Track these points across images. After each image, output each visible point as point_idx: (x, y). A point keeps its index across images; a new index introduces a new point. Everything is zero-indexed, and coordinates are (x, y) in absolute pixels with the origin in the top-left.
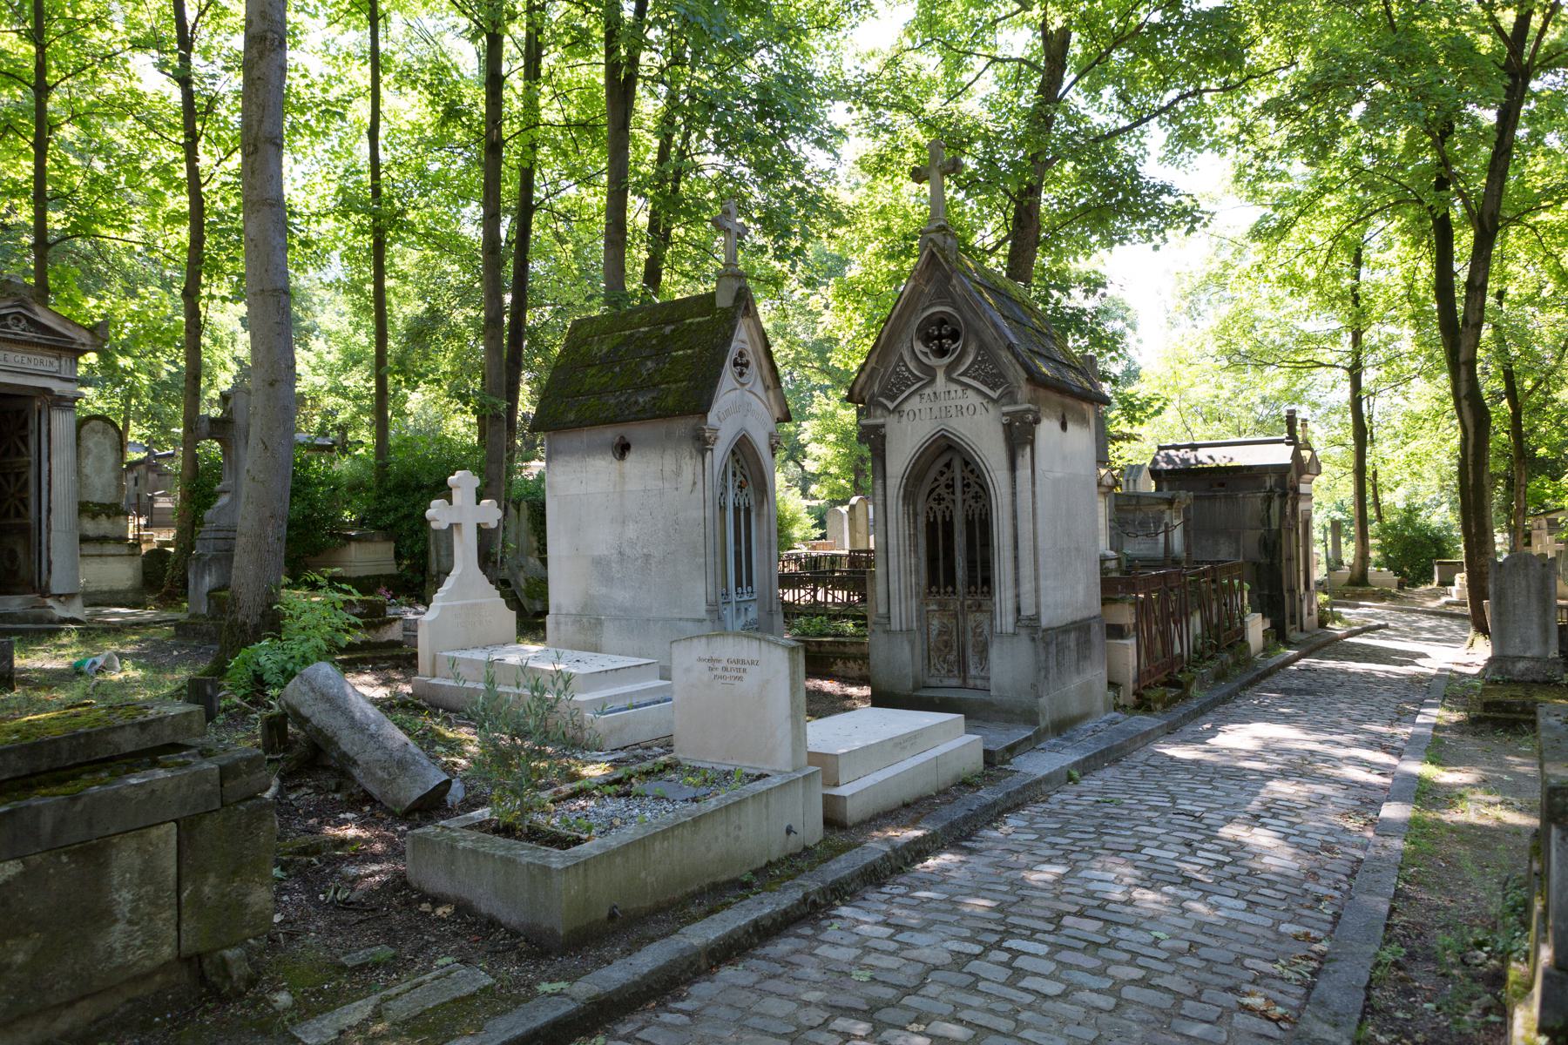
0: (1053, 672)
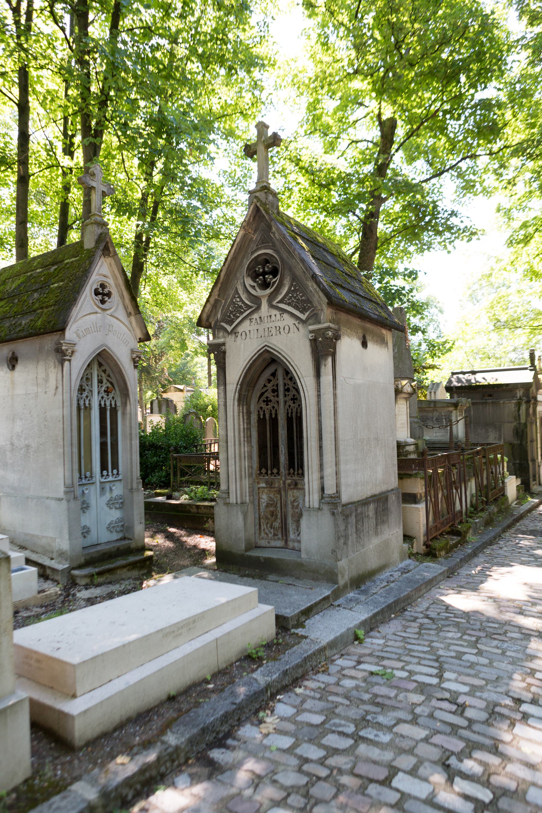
0: (352, 537)
